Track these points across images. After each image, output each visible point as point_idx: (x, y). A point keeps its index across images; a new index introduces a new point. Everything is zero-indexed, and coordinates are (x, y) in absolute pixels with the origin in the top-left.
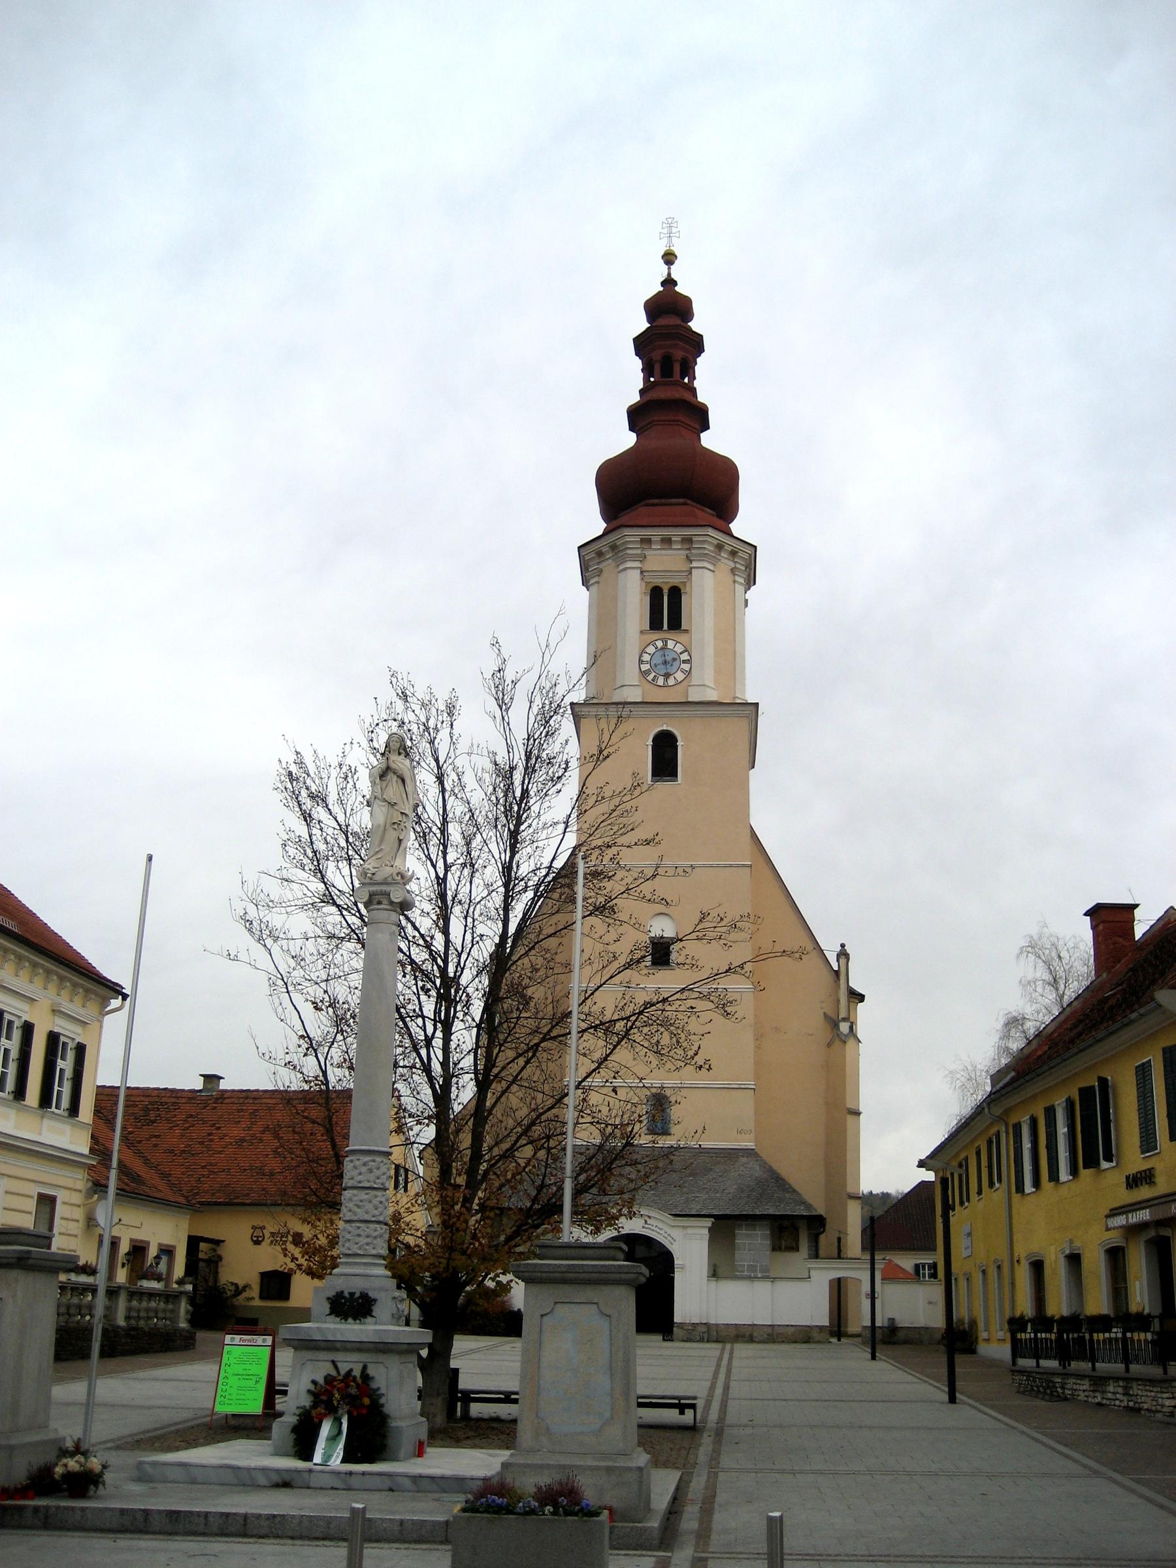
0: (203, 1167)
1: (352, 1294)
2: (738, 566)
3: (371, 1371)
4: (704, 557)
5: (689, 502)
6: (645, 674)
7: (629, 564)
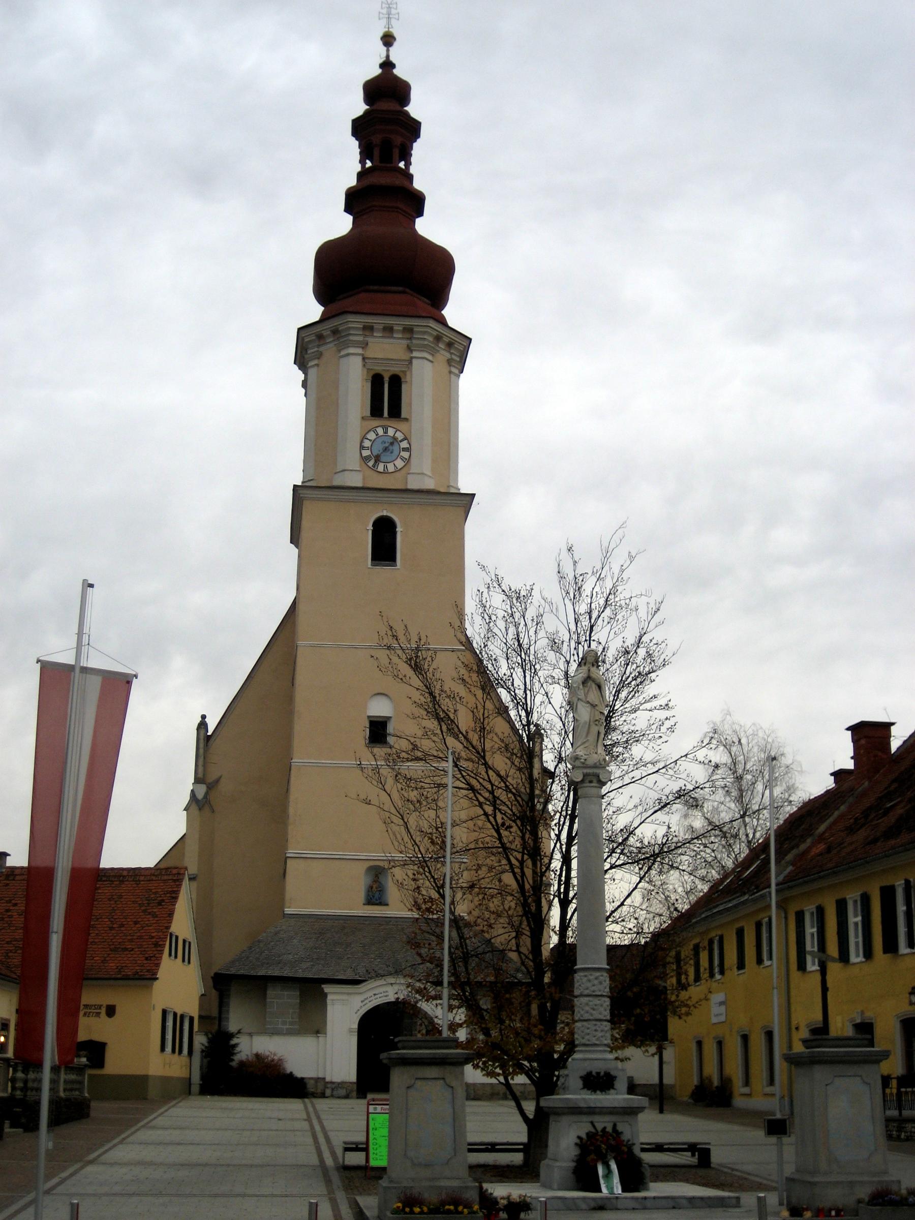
0: (8, 943)
1: (598, 1073)
2: (454, 357)
3: (620, 1128)
4: (423, 348)
5: (408, 290)
6: (365, 459)
7: (351, 350)
